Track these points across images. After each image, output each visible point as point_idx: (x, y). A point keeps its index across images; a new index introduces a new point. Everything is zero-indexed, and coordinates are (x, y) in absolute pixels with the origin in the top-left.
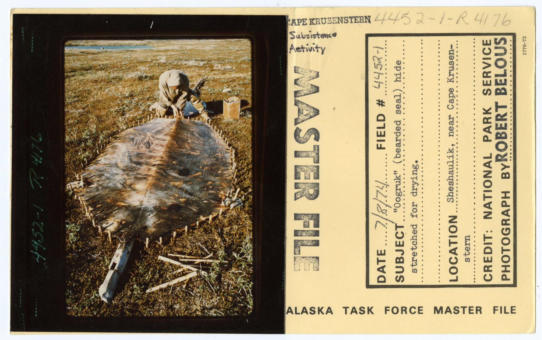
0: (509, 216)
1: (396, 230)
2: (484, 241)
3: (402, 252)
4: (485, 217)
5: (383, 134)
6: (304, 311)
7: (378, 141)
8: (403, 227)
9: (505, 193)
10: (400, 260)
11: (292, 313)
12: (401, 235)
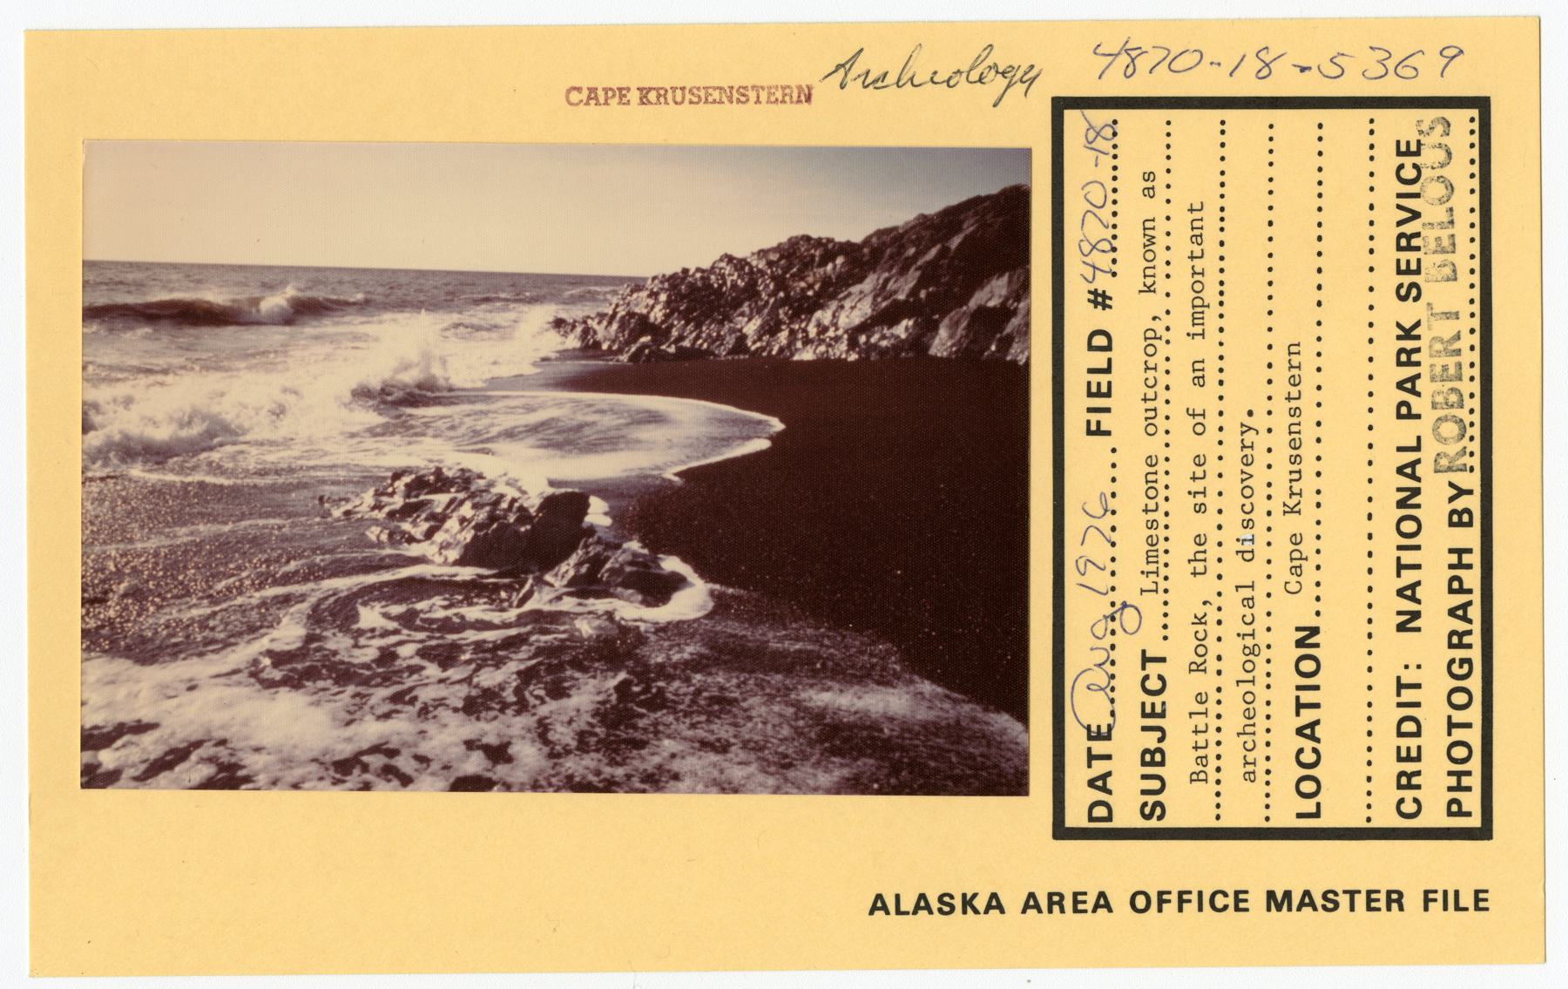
0: (1470, 621)
1: (1144, 668)
2: (1399, 695)
3: (1159, 734)
4: (1401, 627)
5: (1104, 389)
6: (922, 904)
7: (1090, 410)
8: (1163, 660)
9: (1459, 552)
10: (1153, 758)
11: (887, 913)
12: (1158, 685)
